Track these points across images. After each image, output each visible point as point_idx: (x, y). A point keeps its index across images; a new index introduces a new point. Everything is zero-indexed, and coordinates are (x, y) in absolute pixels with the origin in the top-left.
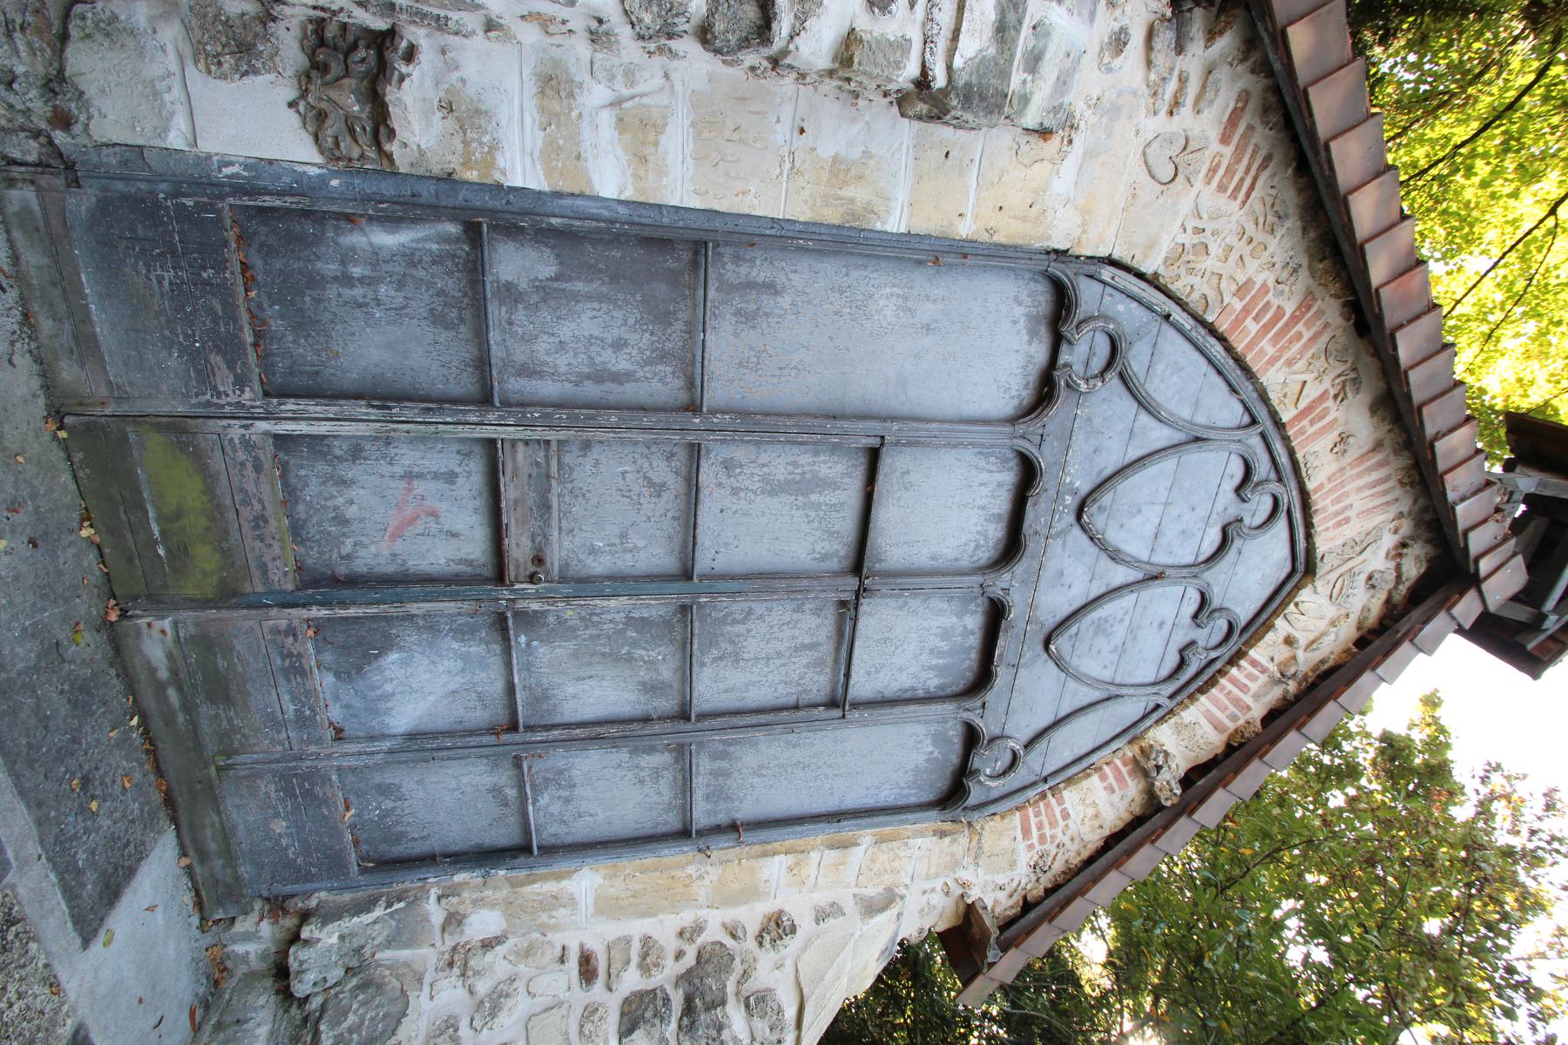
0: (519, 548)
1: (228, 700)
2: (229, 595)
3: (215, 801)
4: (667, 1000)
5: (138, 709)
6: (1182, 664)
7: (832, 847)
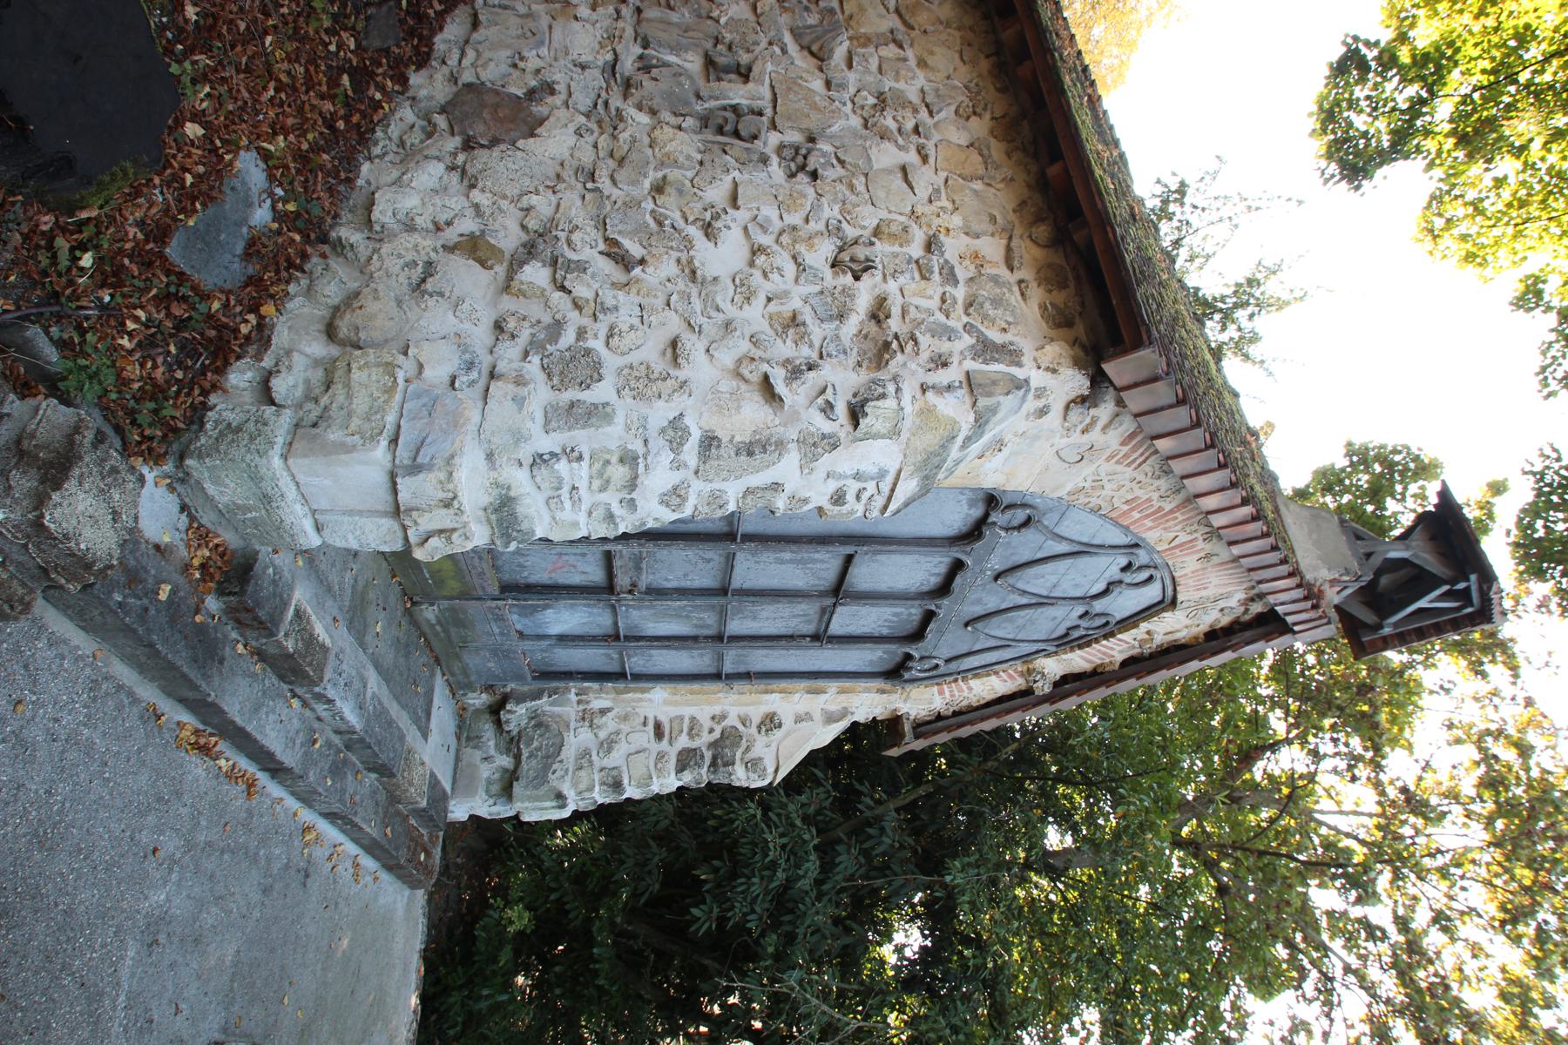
0: (622, 580)
1: (464, 627)
2: (466, 595)
3: (458, 657)
4: (702, 757)
5: (422, 634)
6: (1067, 635)
7: (809, 692)
